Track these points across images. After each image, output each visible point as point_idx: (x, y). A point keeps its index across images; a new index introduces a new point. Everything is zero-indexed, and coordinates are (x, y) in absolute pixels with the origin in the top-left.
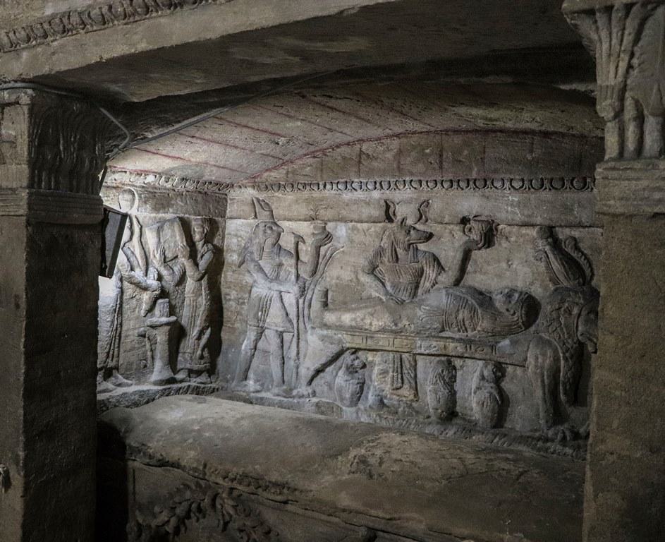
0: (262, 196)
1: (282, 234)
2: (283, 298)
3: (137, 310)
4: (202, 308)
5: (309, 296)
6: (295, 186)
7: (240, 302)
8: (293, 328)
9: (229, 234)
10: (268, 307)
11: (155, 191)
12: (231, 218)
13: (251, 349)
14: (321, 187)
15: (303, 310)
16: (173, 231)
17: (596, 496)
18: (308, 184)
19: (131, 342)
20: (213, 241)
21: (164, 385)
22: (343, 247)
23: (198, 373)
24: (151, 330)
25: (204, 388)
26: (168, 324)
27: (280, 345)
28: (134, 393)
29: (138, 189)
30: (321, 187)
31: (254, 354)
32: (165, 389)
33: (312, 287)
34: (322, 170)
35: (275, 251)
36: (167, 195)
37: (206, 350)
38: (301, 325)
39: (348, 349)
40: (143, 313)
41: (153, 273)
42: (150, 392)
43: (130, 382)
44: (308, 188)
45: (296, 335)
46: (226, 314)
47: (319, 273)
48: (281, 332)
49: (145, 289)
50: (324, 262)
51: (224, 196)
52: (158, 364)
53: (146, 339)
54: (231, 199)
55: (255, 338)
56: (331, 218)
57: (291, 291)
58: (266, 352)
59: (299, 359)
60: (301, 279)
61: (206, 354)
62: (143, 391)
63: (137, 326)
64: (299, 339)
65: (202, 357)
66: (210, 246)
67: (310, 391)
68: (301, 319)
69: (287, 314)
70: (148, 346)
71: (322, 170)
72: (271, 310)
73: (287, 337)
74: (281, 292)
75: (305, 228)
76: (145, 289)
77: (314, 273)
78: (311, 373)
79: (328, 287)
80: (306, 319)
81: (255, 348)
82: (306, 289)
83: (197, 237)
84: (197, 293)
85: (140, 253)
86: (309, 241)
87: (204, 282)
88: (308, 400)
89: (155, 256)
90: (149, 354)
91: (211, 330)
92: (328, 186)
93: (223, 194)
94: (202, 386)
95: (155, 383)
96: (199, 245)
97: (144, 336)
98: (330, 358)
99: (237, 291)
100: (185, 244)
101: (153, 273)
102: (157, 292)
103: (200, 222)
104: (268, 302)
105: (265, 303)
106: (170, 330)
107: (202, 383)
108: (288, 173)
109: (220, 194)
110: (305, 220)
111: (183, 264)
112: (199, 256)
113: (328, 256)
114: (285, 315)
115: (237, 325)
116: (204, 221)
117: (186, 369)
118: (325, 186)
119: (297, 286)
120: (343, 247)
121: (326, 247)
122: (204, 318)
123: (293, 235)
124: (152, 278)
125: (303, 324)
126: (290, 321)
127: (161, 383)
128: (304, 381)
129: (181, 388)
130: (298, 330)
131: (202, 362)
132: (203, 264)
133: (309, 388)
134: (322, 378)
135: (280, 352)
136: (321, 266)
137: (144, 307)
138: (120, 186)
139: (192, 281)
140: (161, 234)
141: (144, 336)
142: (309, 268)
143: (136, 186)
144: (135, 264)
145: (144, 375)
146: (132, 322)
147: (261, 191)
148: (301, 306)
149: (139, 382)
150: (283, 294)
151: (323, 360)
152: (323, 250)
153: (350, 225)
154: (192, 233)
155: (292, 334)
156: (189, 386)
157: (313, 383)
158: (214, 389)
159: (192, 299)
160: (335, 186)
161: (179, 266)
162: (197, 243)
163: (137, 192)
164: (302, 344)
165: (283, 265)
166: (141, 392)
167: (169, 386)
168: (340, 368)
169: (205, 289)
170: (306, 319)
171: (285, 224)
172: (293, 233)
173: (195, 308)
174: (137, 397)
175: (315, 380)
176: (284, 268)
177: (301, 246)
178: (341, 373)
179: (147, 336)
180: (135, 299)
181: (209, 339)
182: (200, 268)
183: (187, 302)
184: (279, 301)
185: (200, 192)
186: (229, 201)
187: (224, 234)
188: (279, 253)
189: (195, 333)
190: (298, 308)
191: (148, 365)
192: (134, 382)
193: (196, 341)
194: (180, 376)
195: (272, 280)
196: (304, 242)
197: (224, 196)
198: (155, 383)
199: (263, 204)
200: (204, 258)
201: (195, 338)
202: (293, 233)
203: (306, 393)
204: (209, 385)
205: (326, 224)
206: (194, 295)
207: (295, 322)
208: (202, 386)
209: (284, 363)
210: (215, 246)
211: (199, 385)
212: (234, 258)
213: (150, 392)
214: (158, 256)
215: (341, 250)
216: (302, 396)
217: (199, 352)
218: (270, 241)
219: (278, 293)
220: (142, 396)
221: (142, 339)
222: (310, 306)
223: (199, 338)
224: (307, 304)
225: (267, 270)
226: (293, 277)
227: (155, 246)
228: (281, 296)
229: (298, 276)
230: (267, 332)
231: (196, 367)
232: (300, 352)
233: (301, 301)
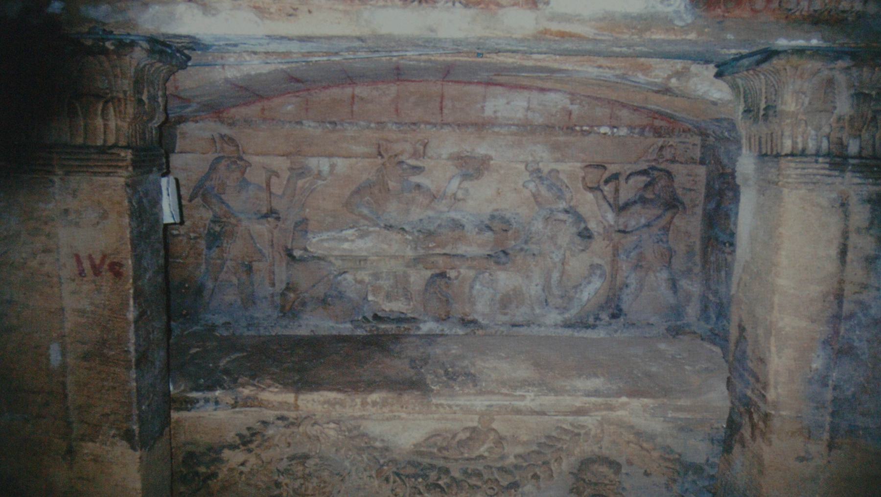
12: (181, 152)
34: (307, 109)
71: (307, 109)
75: (280, 164)
108: (263, 110)
110: (283, 155)
172: (264, 168)
186: (178, 136)
202: (264, 168)
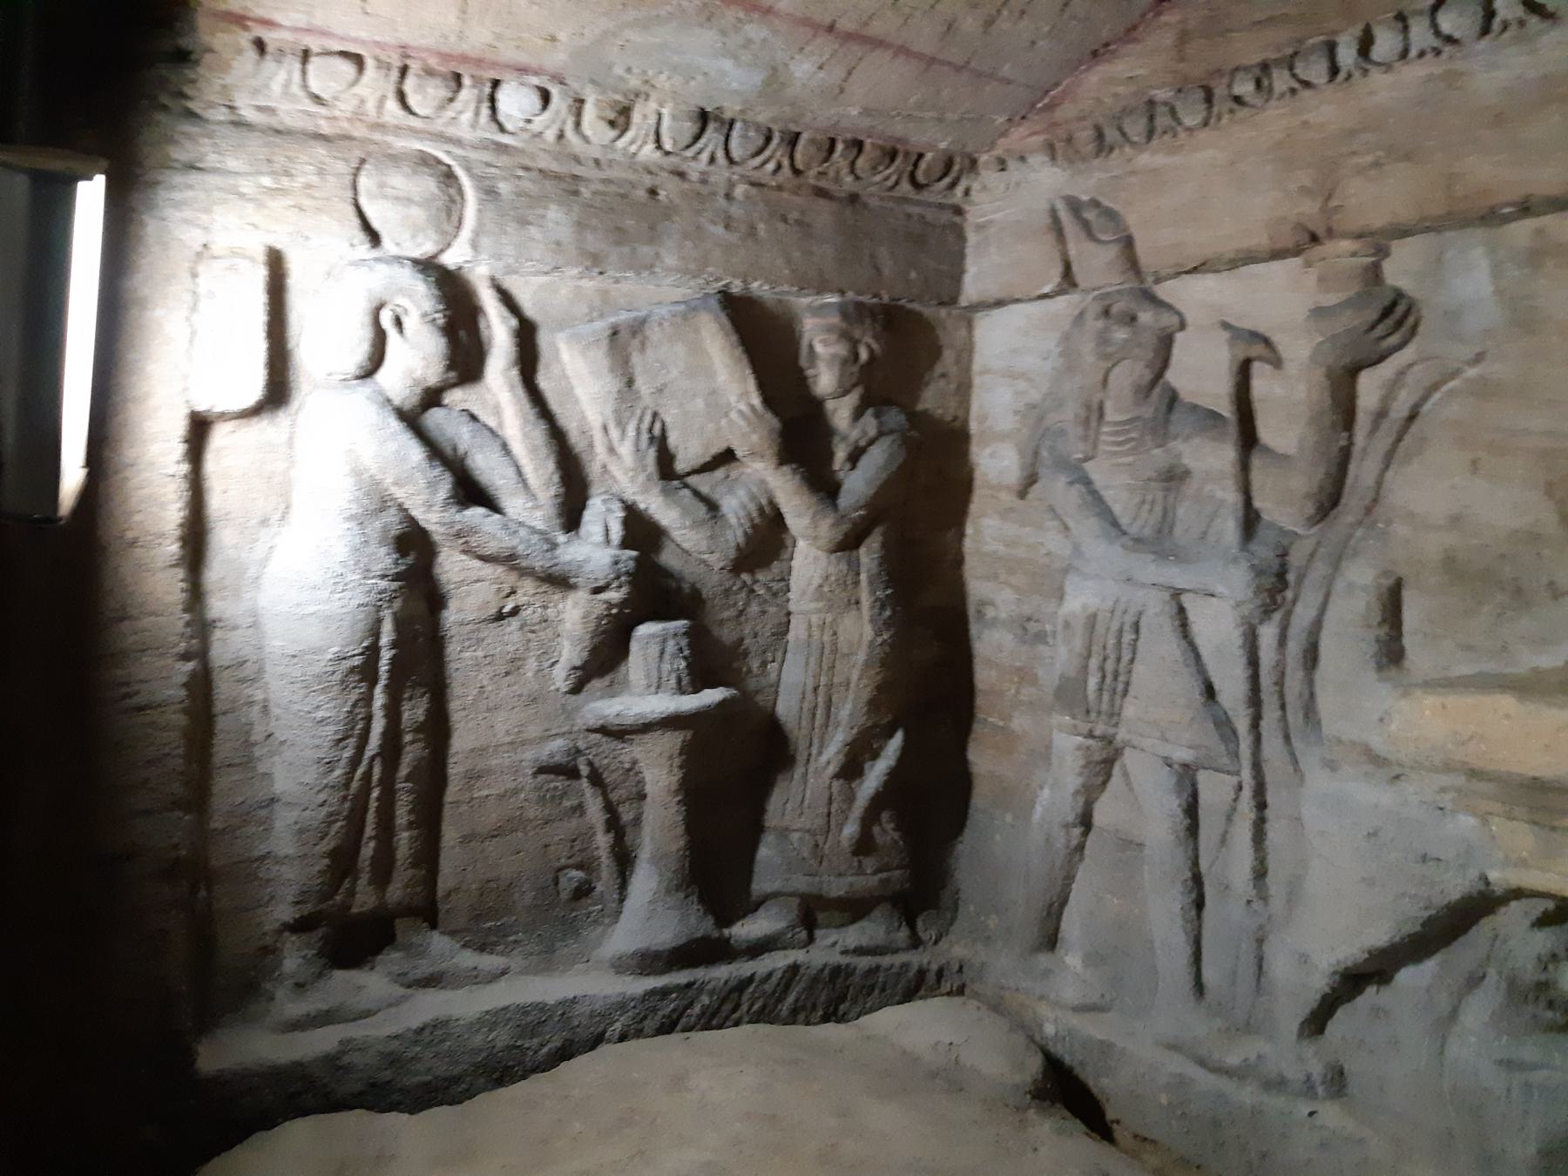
0: (1087, 183)
1: (1179, 336)
2: (1192, 616)
3: (532, 665)
4: (861, 657)
5: (1303, 614)
6: (1220, 91)
7: (1030, 631)
8: (1235, 755)
9: (986, 371)
10: (1126, 658)
11: (578, 171)
13: (1067, 826)
14: (1347, 55)
15: (1280, 683)
16: (696, 349)
17: (838, 172)
18: (1278, 62)
19: (501, 797)
20: (915, 395)
21: (662, 973)
22: (1478, 359)
23: (854, 908)
24: (608, 744)
25: (873, 971)
26: (672, 722)
27: (1182, 822)
28: (493, 1019)
29: (474, 155)
30: (1347, 55)
31: (1081, 848)
32: (664, 993)
33: (1320, 569)
35: (1147, 411)
36: (641, 194)
37: (885, 816)
38: (1272, 746)
39: (1518, 894)
40: (560, 678)
41: (602, 517)
42: (580, 1009)
43: (489, 962)
44: (1281, 80)
45: (1247, 793)
46: (984, 676)
47: (1352, 501)
48: (1186, 766)
49: (560, 581)
50: (1383, 441)
51: (946, 217)
52: (645, 882)
53: (585, 783)
54: (980, 228)
55: (1080, 781)
56: (1405, 213)
57: (1220, 589)
58: (1130, 845)
59: (1264, 897)
60: (1262, 533)
61: (887, 832)
62: (541, 1007)
63: (533, 731)
64: (1261, 806)
65: (864, 845)
66: (895, 418)
67: (1317, 1069)
68: (1270, 715)
69: (1210, 692)
70: (595, 811)
72: (1138, 668)
73: (1214, 790)
74: (1177, 594)
76: (560, 581)
77: (1329, 501)
78: (1319, 983)
79: (1402, 571)
80: (1295, 718)
81: (1086, 821)
82: (1291, 577)
83: (824, 380)
84: (841, 596)
85: (525, 435)
86: (1298, 349)
87: (869, 555)
88: (1304, 1108)
89: (611, 450)
90: (603, 841)
91: (906, 740)
92: (1385, 43)
93: (941, 206)
94: (865, 962)
95: (621, 966)
96: (841, 413)
97: (571, 772)
98: (1410, 928)
99: (1017, 589)
100: (756, 400)
101: (602, 517)
102: (614, 595)
103: (835, 319)
104: (1128, 637)
105: (1111, 642)
106: (687, 750)
107: (860, 951)
109: (918, 203)
110: (1277, 255)
111: (763, 482)
112: (840, 454)
113: (1400, 409)
114: (1197, 697)
115: (1019, 723)
116: (854, 314)
117: (791, 895)
118: (1365, 44)
119: (1244, 565)
120: (1478, 359)
121: (1386, 370)
122: (866, 694)
123: (1226, 335)
124: (599, 538)
125: (1280, 741)
126: (1224, 726)
127: (648, 962)
128: (1291, 1013)
129: (751, 979)
130: (1257, 766)
131: (870, 863)
132: (857, 484)
133: (1309, 1049)
134: (1377, 1011)
135: (1181, 859)
136: (1363, 471)
137: (570, 653)
138: (359, 131)
139: (814, 552)
140: (636, 359)
141: (571, 772)
142: (1303, 481)
143: (458, 142)
144: (487, 466)
145: (570, 928)
146: (501, 716)
147: (1083, 159)
148: (1267, 656)
149: (547, 961)
150: (1187, 601)
151: (1380, 935)
152: (1369, 386)
153: (1521, 231)
154: (803, 362)
155: (1234, 780)
156: (794, 969)
157: (1341, 1023)
158: (922, 973)
159: (815, 619)
160: (1420, 33)
161: (742, 493)
162: (830, 405)
163: (468, 169)
164: (1276, 832)
165: (1187, 473)
166: (524, 1010)
167: (680, 977)
168: (1474, 981)
169: (871, 583)
170: (1295, 718)
171: (1188, 295)
173: (829, 654)
174: (502, 1037)
175: (1341, 1013)
176: (1191, 487)
177: (1263, 383)
178: (1479, 1010)
179: (584, 770)
180: (514, 623)
181: (893, 775)
182: (844, 501)
183: (797, 632)
184: (1168, 627)
185: (821, 193)
187: (966, 370)
188: (1167, 421)
189: (832, 752)
190: (1253, 662)
191: (599, 888)
192: (516, 961)
193: (836, 785)
194: (747, 929)
195: (1138, 540)
196: (1277, 362)
197: (946, 217)
198: (621, 966)
199: (1090, 215)
200: (864, 462)
201: (832, 769)
203: (1294, 1073)
204: (902, 958)
205: (1382, 252)
206: (820, 605)
207: (1242, 724)
208: (865, 962)
209: (1199, 904)
210: (917, 419)
211: (844, 960)
212: (1006, 463)
213: (580, 1009)
214: (625, 449)
215: (1472, 372)
216: (1277, 1084)
217: (850, 830)
218: (1127, 375)
219: (1166, 595)
220: (533, 1030)
221: (559, 783)
222: (1311, 657)
223: (851, 770)
224: (1295, 647)
225: (1119, 500)
226: (1229, 528)
227: (609, 410)
228: (1182, 610)
229: (1250, 521)
230: (1129, 758)
231: (837, 888)
232: (1272, 864)
233: (1268, 634)
